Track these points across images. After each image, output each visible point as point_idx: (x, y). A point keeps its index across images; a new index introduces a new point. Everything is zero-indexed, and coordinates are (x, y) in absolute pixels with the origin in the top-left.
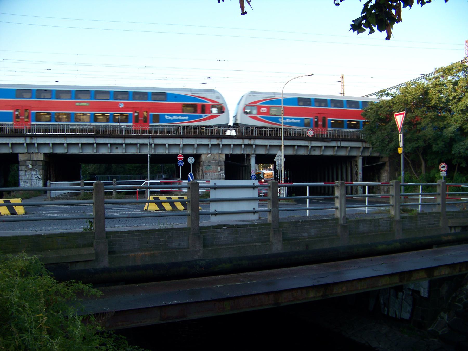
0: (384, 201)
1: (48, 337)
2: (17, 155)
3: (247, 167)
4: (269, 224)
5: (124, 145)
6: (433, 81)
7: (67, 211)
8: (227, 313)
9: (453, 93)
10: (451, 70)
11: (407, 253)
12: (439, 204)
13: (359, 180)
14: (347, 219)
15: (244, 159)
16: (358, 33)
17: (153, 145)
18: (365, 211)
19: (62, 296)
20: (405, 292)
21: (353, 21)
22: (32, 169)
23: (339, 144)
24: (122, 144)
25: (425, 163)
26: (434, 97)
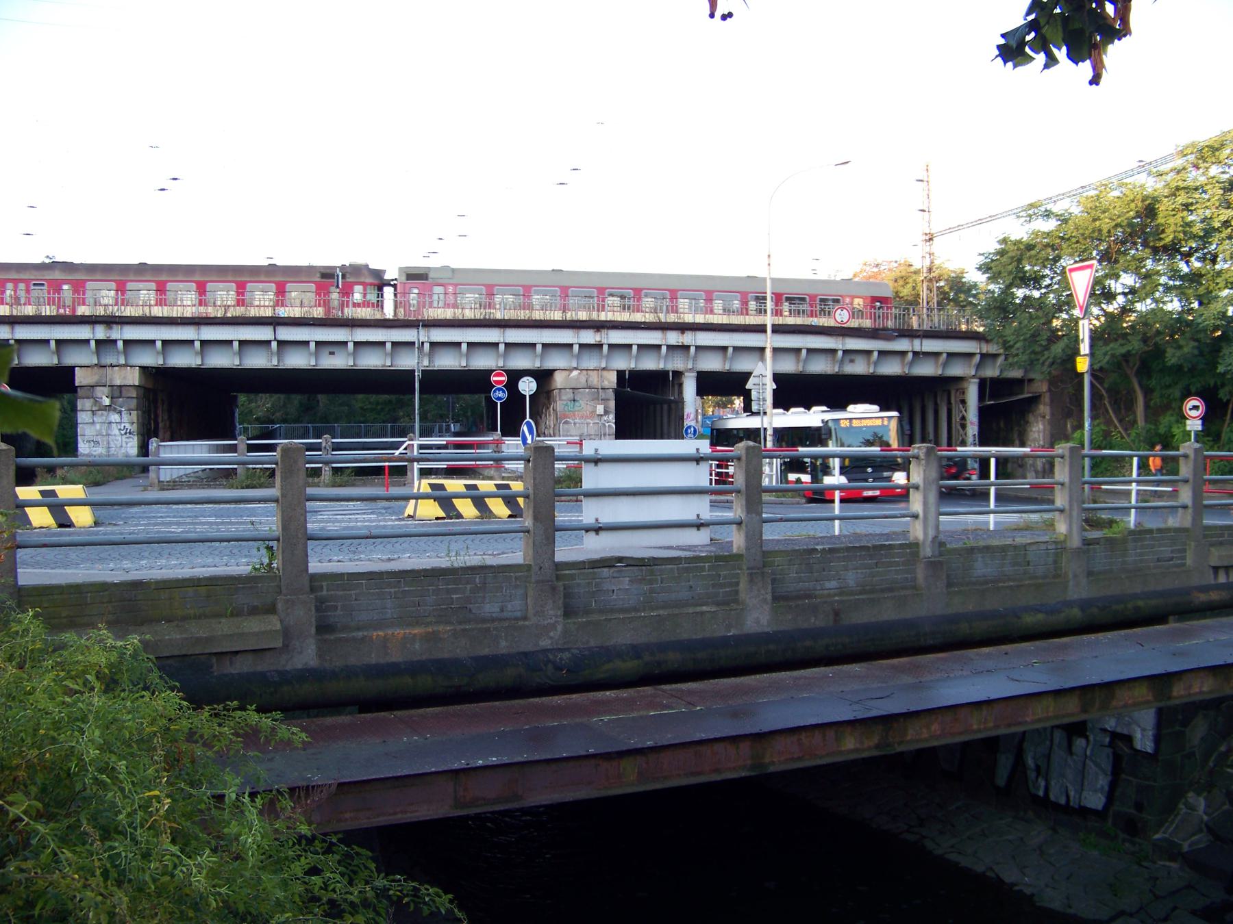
0: (1040, 497)
1: (175, 849)
2: (71, 370)
3: (673, 406)
4: (738, 557)
5: (351, 345)
6: (1168, 178)
7: (202, 519)
8: (629, 790)
9: (1223, 211)
10: (1217, 150)
11: (1100, 636)
12: (1185, 507)
13: (970, 439)
14: (942, 544)
15: (664, 382)
16: (1015, 67)
17: (427, 346)
18: (988, 523)
19: (205, 745)
20: (1091, 738)
21: (1003, 36)
22: (109, 408)
23: (917, 345)
25: (1145, 397)
26: (1171, 220)
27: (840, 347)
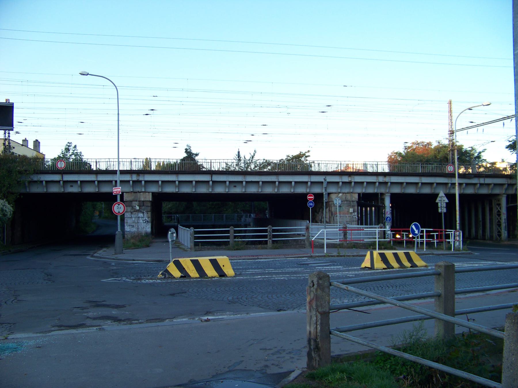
23: (482, 181)
24: (242, 182)
27: (450, 182)
